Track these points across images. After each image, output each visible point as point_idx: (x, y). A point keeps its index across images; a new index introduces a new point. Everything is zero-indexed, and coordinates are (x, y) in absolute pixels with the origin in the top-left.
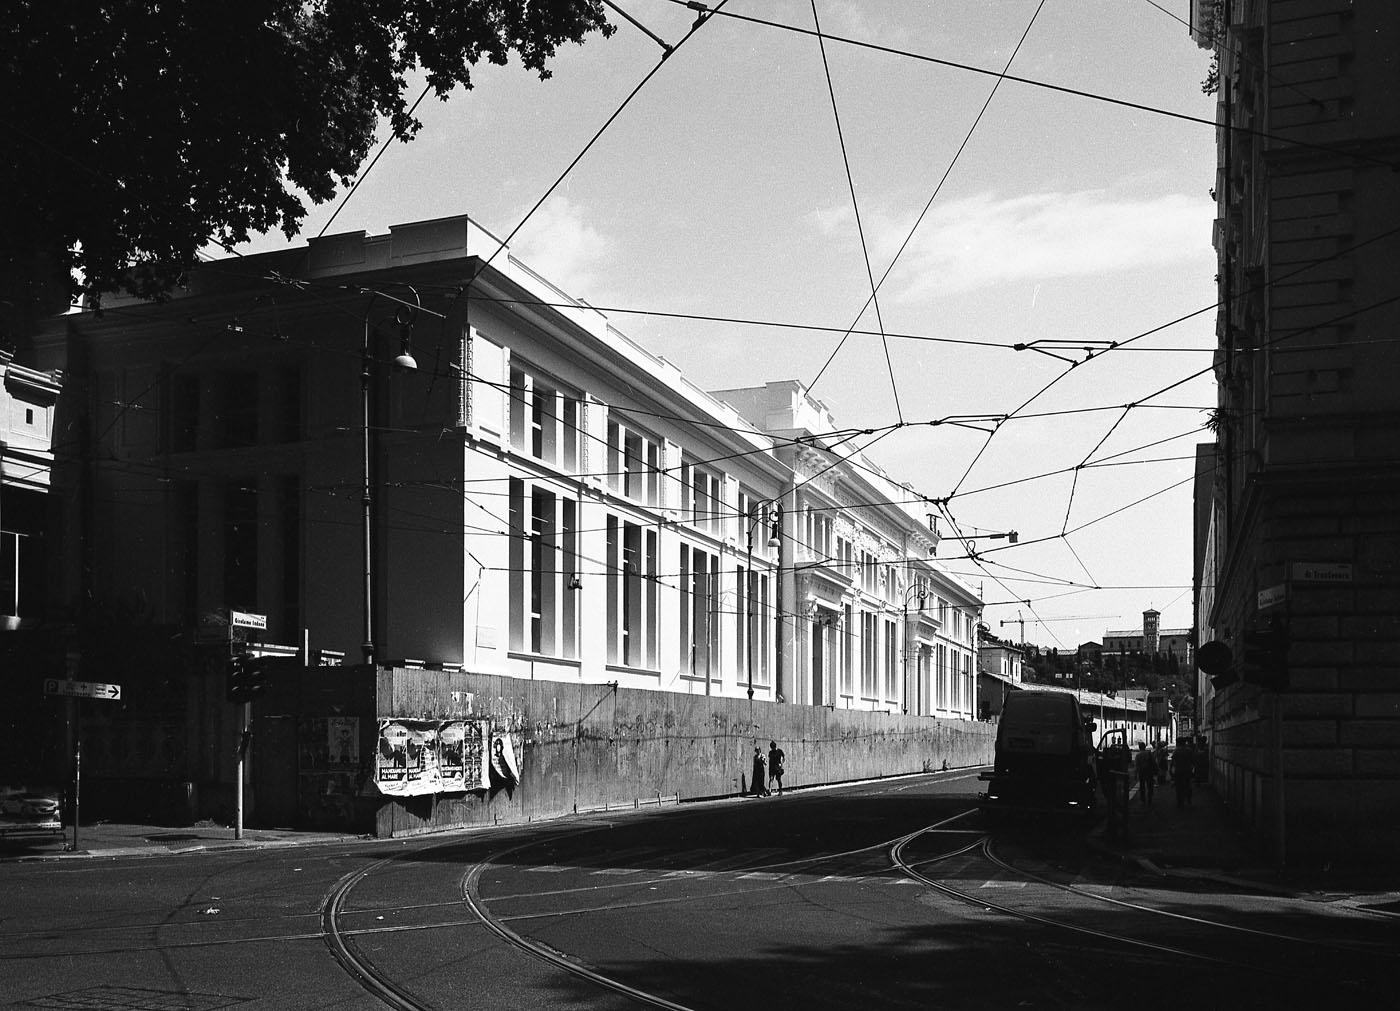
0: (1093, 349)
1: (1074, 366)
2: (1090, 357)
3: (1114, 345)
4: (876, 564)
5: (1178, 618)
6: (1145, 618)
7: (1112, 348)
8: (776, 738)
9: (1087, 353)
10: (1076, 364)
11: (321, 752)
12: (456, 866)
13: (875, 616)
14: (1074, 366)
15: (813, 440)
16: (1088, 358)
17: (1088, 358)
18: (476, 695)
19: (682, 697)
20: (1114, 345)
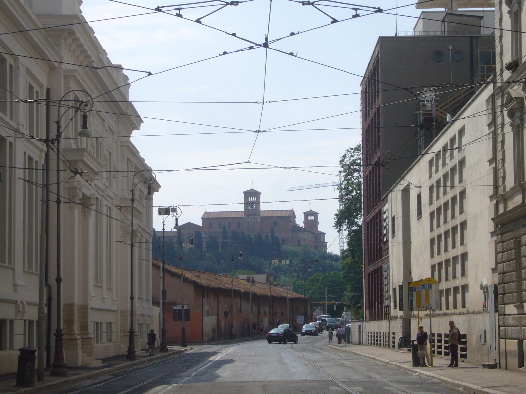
0: (358, 9)
1: (332, 22)
2: (356, 16)
3: (379, 10)
4: (25, 168)
5: (263, 207)
6: (246, 198)
7: (376, 12)
8: (236, 364)
9: (354, 12)
10: (335, 21)
11: (511, 309)
12: (427, 34)
13: (11, 143)
14: (332, 22)
15: (179, 9)
16: (354, 17)
17: (354, 17)
18: (349, 308)
19: (404, 346)
20: (379, 10)
